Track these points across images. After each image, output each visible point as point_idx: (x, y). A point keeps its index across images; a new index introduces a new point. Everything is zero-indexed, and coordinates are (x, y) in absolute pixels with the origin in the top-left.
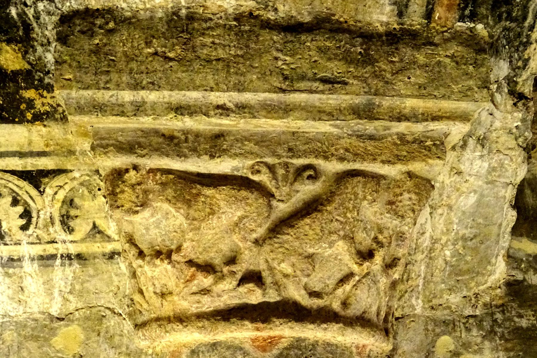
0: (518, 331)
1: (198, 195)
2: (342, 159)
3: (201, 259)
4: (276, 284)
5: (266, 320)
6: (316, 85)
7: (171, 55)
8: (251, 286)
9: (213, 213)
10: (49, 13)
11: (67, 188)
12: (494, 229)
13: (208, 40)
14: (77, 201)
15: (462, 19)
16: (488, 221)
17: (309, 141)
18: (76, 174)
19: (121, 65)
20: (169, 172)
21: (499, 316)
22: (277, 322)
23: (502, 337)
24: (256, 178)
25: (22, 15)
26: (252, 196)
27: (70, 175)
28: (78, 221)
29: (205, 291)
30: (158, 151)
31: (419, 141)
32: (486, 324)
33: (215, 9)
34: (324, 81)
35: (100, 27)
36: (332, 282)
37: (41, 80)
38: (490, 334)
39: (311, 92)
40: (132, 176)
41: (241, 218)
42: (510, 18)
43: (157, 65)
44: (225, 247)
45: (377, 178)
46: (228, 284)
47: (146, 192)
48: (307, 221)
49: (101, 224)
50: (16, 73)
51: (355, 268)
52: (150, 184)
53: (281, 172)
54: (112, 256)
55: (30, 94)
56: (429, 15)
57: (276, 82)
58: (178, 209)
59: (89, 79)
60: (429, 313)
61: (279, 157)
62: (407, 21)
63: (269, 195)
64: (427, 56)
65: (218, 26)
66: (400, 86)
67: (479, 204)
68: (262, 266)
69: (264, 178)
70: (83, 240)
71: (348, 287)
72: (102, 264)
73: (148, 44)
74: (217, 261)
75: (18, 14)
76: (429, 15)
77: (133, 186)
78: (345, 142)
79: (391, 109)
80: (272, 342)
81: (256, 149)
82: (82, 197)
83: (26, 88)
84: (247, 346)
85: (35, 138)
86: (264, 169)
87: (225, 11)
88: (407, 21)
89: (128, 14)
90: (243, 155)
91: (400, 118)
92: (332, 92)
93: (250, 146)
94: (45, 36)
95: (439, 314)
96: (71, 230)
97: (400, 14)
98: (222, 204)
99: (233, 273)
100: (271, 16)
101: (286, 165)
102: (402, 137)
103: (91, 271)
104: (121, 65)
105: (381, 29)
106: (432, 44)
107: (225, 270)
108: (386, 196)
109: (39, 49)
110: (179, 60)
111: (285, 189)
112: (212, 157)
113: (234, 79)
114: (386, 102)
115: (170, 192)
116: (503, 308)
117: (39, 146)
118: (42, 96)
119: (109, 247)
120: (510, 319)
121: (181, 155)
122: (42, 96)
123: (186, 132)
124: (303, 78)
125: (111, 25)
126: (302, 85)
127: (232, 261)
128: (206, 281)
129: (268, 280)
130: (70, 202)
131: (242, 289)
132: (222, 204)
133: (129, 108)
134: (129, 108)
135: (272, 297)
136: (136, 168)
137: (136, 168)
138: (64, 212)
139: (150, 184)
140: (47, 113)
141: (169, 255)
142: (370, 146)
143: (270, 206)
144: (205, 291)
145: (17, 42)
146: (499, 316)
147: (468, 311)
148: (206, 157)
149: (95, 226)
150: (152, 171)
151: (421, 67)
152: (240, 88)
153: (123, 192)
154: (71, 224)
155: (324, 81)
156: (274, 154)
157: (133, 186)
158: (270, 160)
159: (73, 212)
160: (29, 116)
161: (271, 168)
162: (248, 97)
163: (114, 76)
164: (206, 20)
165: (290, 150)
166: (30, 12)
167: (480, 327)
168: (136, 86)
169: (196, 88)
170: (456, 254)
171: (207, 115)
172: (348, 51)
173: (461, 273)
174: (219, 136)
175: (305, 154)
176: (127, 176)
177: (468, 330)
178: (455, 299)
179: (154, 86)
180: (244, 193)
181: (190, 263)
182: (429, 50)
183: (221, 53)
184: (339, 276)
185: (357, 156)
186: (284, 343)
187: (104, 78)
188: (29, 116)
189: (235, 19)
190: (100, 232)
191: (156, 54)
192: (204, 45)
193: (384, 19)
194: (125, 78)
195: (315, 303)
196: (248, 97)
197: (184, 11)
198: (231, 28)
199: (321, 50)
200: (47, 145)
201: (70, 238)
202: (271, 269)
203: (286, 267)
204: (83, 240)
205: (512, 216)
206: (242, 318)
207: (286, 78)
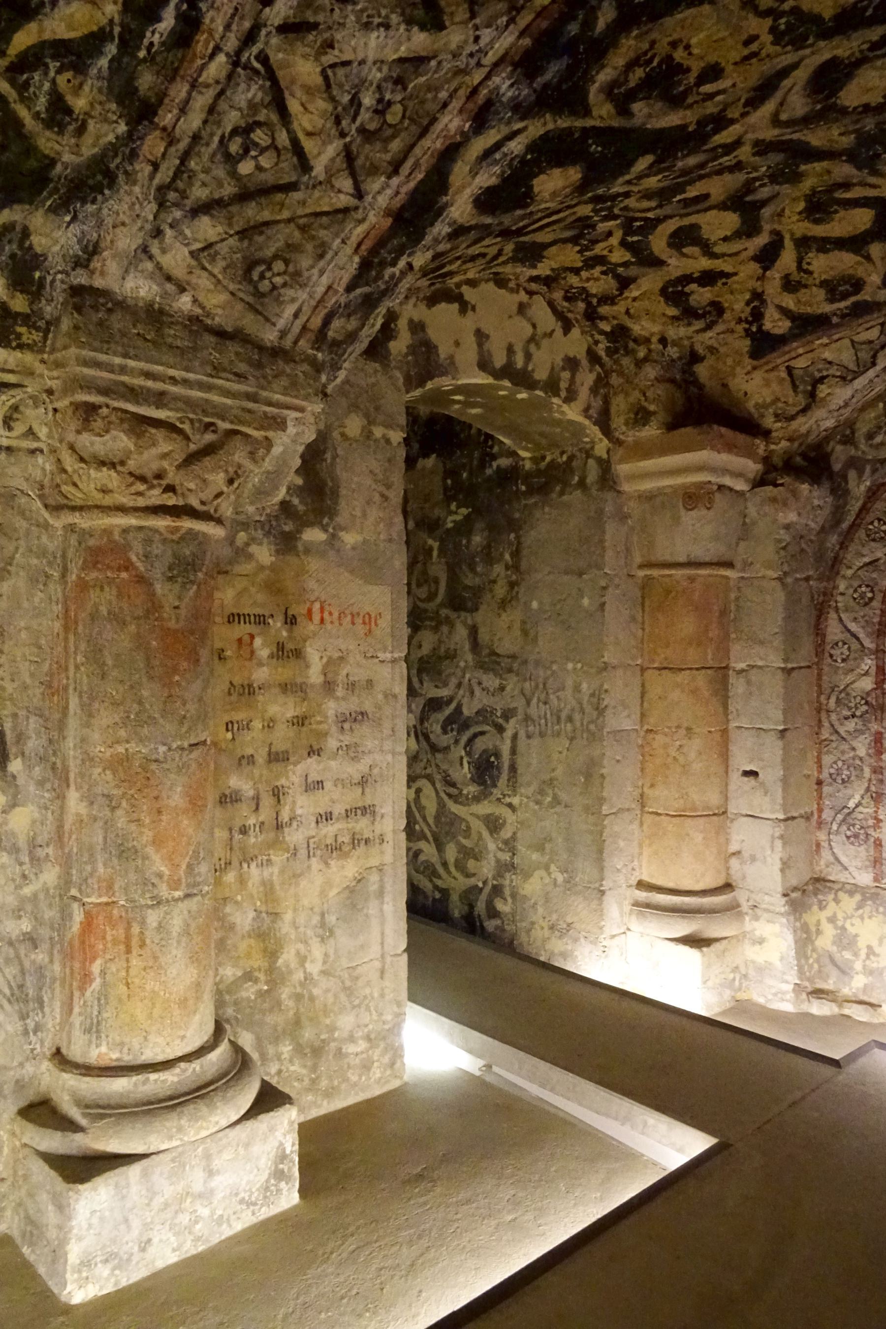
0: (283, 533)
1: (146, 431)
2: (232, 422)
3: (138, 472)
4: (183, 494)
5: (178, 516)
6: (231, 376)
7: (148, 337)
8: (171, 494)
9: (154, 445)
10: (62, 282)
11: (18, 398)
12: (286, 470)
13: (172, 332)
14: (21, 408)
15: (312, 348)
16: (285, 462)
17: (215, 407)
18: (29, 390)
19: (117, 338)
20: (126, 412)
21: (274, 523)
22: (185, 518)
23: (274, 536)
24: (181, 426)
25: (42, 279)
26: (179, 438)
27: (24, 389)
28: (17, 423)
29: (139, 494)
30: (124, 397)
31: (274, 418)
32: (267, 528)
33: (176, 309)
34: (236, 374)
35: (103, 305)
36: (211, 497)
37: (35, 323)
38: (268, 534)
39: (228, 380)
40: (104, 411)
41: (171, 451)
42: (336, 354)
43: (139, 342)
44: (155, 466)
45: (247, 436)
46: (156, 492)
47: (110, 423)
48: (208, 458)
49: (36, 428)
50: (18, 314)
51: (225, 489)
52: (113, 418)
53: (197, 425)
54: (33, 452)
55: (22, 330)
56: (296, 342)
57: (209, 369)
58: (129, 438)
59: (97, 344)
60: (234, 516)
61: (197, 414)
62: (283, 342)
63: (187, 438)
64: (292, 369)
65: (177, 323)
66: (274, 386)
67: (284, 452)
68: (177, 482)
69: (186, 427)
70: (17, 438)
71: (219, 500)
72: (22, 456)
73: (134, 326)
74: (149, 475)
75: (40, 278)
76: (296, 342)
77: (103, 418)
78: (235, 412)
79: (266, 398)
80: (177, 529)
81: (184, 406)
82: (26, 406)
83: (21, 326)
84: (162, 530)
85: (11, 360)
86: (187, 422)
87: (182, 312)
88: (283, 342)
89: (120, 298)
90: (177, 410)
91: (270, 404)
92: (239, 383)
93: (180, 404)
94: (51, 295)
95: (242, 518)
96: (10, 429)
97: (281, 338)
98: (161, 440)
99: (160, 485)
100: (209, 322)
101: (200, 421)
102: (265, 413)
103: (13, 460)
104: (117, 338)
105: (269, 344)
106: (295, 361)
107: (155, 482)
108: (249, 448)
109: (44, 302)
110: (154, 342)
111: (198, 437)
112: (157, 408)
113: (185, 363)
114: (264, 394)
115: (126, 426)
116: (277, 517)
117: (11, 365)
118: (30, 333)
119: (35, 445)
120: (280, 526)
121: (138, 403)
122: (30, 333)
123: (141, 387)
124: (225, 370)
125: (110, 305)
126: (223, 375)
127: (159, 476)
128: (142, 487)
129: (179, 492)
130: (15, 408)
131: (165, 496)
132: (161, 440)
133: (117, 368)
134: (117, 368)
135: (181, 502)
136: (107, 406)
137: (107, 406)
138: (8, 414)
139: (113, 418)
140: (28, 345)
141: (113, 465)
142: (248, 417)
143: (188, 446)
144: (139, 494)
145: (28, 293)
146: (274, 523)
147: (258, 518)
148: (153, 407)
149: (30, 428)
150: (115, 409)
151: (288, 375)
152: (187, 369)
153: (95, 421)
154: (12, 424)
155: (236, 374)
156: (194, 412)
157: (103, 418)
158: (191, 416)
159: (15, 416)
160: (14, 344)
161: (192, 421)
162: (191, 376)
163: (112, 345)
164: (172, 316)
165: (203, 411)
166: (49, 278)
167: (263, 529)
168: (126, 356)
169: (162, 364)
170: (260, 481)
171: (164, 382)
172: (250, 357)
173: (260, 493)
174: (162, 394)
175: (213, 415)
176: (100, 411)
177: (256, 530)
178: (251, 509)
179: (136, 358)
180: (175, 436)
181: (131, 474)
182: (292, 365)
183: (179, 343)
184: (215, 493)
185: (241, 422)
186: (183, 531)
187: (106, 346)
188: (14, 344)
189: (189, 320)
190: (33, 434)
191: (138, 334)
192: (169, 335)
193: (271, 338)
194: (120, 349)
195: (204, 508)
196: (191, 376)
197: (156, 306)
198: (185, 326)
199: (237, 354)
200: (17, 366)
201: (7, 434)
202: (182, 485)
203: (192, 486)
204: (17, 438)
205: (298, 462)
206: (165, 514)
207: (215, 368)
